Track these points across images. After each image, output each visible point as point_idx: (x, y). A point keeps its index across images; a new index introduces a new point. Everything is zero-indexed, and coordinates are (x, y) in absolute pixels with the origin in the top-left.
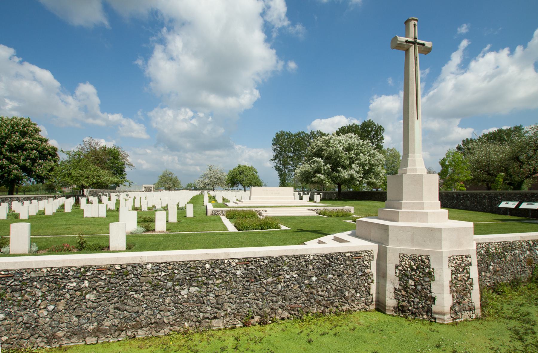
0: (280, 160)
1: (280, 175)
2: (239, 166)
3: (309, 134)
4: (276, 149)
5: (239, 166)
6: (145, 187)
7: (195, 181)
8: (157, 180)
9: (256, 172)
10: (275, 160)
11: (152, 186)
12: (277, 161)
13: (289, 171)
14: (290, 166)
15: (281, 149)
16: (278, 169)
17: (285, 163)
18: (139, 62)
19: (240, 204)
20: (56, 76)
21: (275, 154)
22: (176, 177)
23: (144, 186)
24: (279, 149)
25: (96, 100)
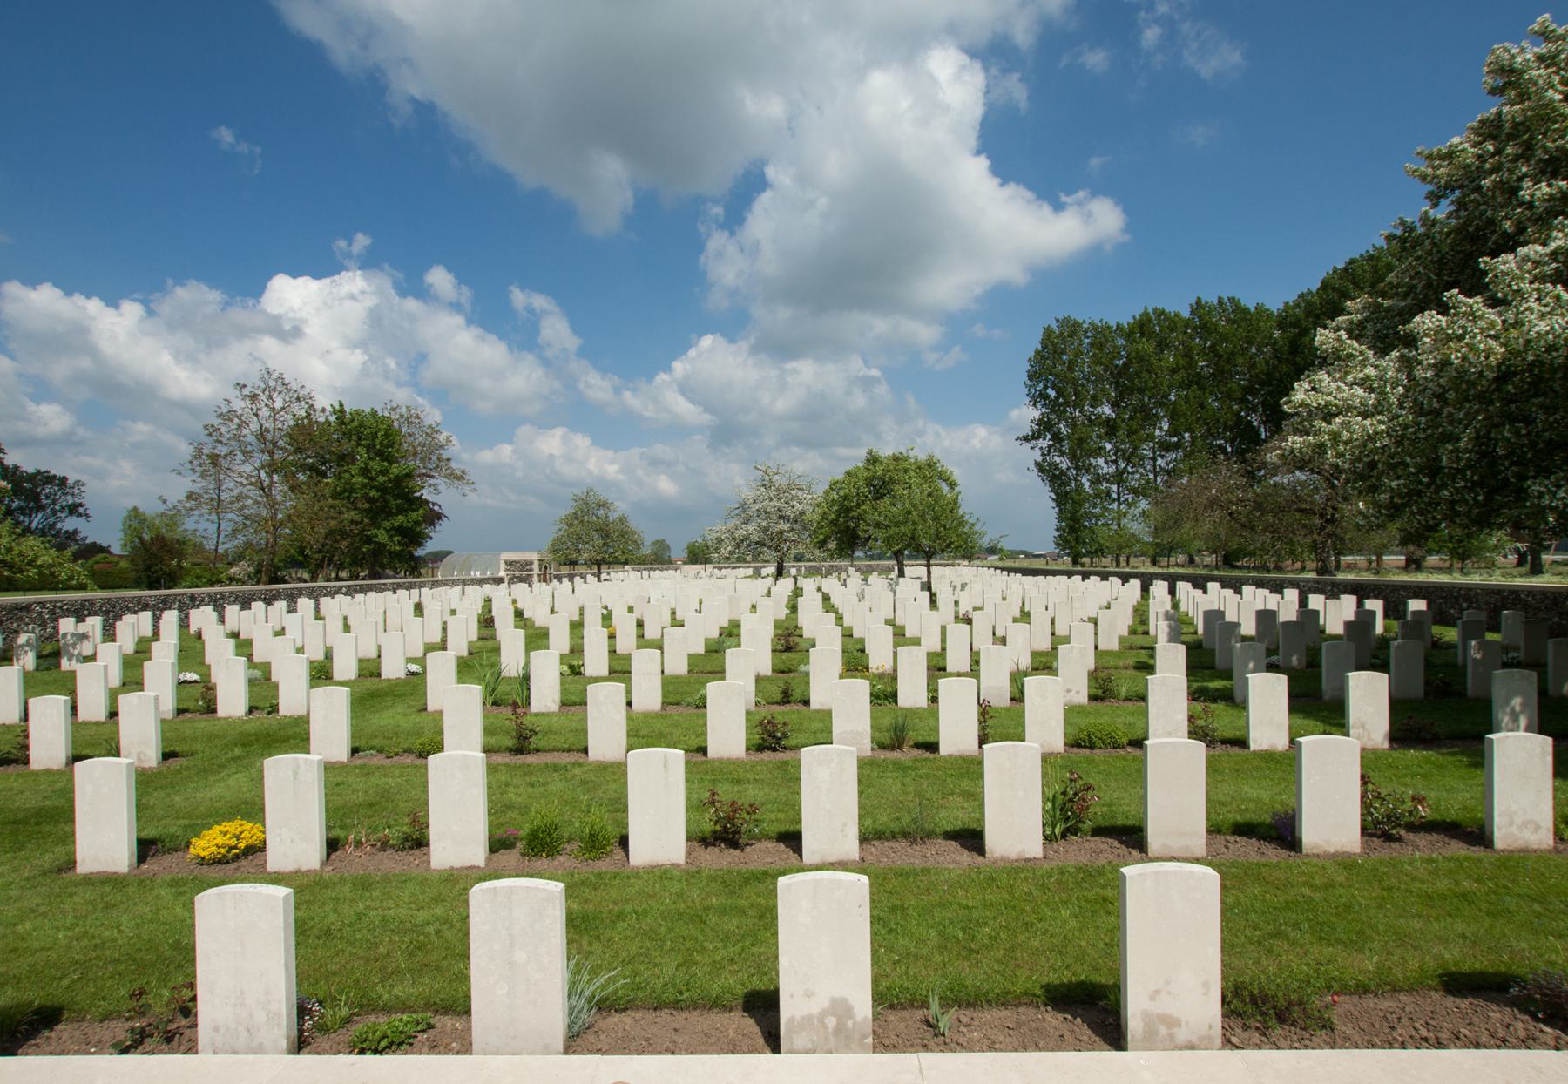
0: (1057, 438)
1: (1061, 499)
2: (873, 460)
3: (1186, 314)
4: (1044, 396)
5: (873, 460)
6: (509, 563)
7: (715, 528)
8: (549, 533)
9: (952, 485)
10: (1034, 436)
11: (534, 556)
12: (1043, 443)
13: (1097, 480)
14: (1101, 461)
15: (1060, 393)
16: (1049, 472)
17: (1081, 451)
18: (1251, 665)
19: (47, 803)
20: (576, 329)
21: (1037, 415)
22: (623, 520)
23: (506, 556)
24: (1052, 393)
25: (573, 342)
